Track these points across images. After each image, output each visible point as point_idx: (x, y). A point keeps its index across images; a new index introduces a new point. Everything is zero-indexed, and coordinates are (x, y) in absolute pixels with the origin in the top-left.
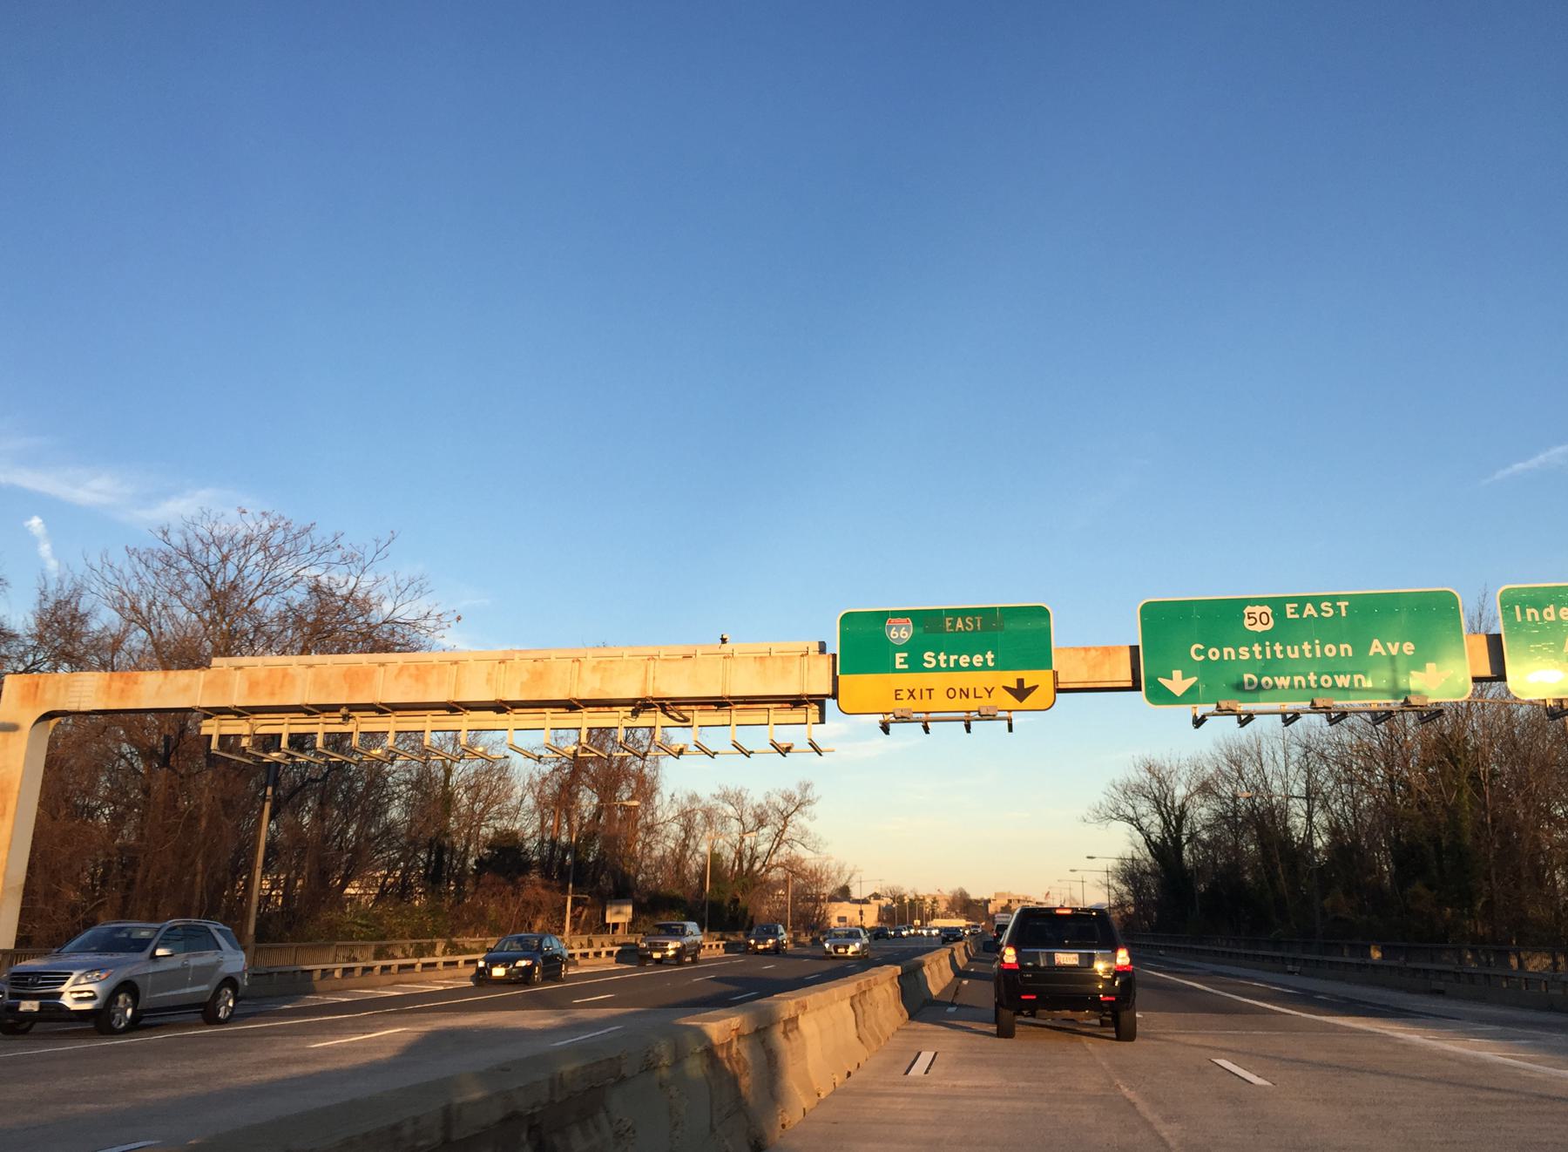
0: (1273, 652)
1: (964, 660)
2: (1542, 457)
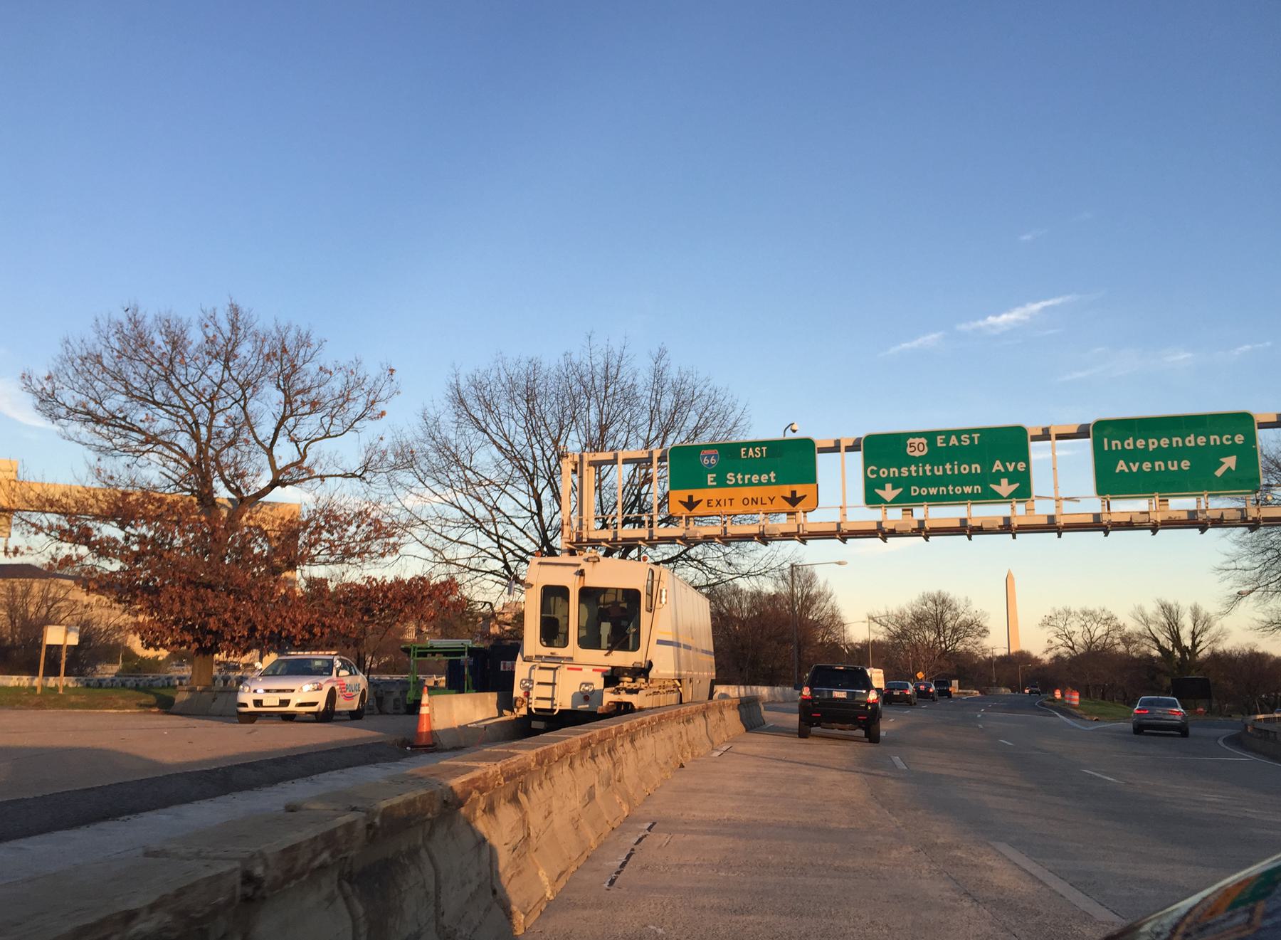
0: (924, 471)
1: (755, 478)
2: (920, 341)
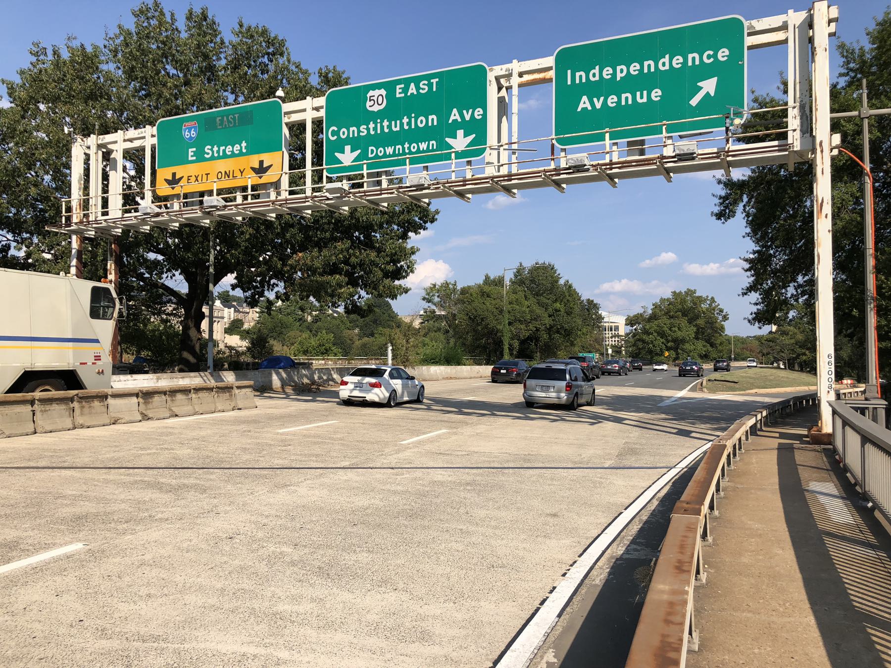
0: (382, 127)
1: (229, 149)
